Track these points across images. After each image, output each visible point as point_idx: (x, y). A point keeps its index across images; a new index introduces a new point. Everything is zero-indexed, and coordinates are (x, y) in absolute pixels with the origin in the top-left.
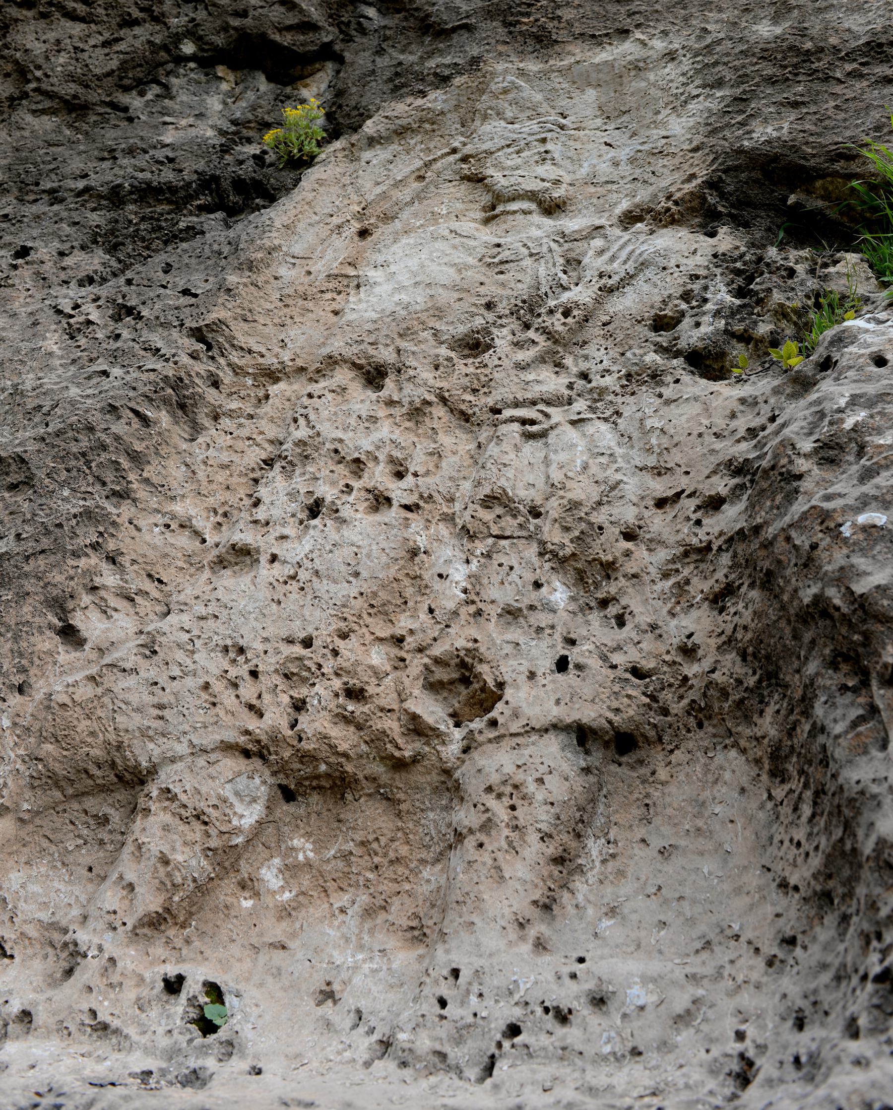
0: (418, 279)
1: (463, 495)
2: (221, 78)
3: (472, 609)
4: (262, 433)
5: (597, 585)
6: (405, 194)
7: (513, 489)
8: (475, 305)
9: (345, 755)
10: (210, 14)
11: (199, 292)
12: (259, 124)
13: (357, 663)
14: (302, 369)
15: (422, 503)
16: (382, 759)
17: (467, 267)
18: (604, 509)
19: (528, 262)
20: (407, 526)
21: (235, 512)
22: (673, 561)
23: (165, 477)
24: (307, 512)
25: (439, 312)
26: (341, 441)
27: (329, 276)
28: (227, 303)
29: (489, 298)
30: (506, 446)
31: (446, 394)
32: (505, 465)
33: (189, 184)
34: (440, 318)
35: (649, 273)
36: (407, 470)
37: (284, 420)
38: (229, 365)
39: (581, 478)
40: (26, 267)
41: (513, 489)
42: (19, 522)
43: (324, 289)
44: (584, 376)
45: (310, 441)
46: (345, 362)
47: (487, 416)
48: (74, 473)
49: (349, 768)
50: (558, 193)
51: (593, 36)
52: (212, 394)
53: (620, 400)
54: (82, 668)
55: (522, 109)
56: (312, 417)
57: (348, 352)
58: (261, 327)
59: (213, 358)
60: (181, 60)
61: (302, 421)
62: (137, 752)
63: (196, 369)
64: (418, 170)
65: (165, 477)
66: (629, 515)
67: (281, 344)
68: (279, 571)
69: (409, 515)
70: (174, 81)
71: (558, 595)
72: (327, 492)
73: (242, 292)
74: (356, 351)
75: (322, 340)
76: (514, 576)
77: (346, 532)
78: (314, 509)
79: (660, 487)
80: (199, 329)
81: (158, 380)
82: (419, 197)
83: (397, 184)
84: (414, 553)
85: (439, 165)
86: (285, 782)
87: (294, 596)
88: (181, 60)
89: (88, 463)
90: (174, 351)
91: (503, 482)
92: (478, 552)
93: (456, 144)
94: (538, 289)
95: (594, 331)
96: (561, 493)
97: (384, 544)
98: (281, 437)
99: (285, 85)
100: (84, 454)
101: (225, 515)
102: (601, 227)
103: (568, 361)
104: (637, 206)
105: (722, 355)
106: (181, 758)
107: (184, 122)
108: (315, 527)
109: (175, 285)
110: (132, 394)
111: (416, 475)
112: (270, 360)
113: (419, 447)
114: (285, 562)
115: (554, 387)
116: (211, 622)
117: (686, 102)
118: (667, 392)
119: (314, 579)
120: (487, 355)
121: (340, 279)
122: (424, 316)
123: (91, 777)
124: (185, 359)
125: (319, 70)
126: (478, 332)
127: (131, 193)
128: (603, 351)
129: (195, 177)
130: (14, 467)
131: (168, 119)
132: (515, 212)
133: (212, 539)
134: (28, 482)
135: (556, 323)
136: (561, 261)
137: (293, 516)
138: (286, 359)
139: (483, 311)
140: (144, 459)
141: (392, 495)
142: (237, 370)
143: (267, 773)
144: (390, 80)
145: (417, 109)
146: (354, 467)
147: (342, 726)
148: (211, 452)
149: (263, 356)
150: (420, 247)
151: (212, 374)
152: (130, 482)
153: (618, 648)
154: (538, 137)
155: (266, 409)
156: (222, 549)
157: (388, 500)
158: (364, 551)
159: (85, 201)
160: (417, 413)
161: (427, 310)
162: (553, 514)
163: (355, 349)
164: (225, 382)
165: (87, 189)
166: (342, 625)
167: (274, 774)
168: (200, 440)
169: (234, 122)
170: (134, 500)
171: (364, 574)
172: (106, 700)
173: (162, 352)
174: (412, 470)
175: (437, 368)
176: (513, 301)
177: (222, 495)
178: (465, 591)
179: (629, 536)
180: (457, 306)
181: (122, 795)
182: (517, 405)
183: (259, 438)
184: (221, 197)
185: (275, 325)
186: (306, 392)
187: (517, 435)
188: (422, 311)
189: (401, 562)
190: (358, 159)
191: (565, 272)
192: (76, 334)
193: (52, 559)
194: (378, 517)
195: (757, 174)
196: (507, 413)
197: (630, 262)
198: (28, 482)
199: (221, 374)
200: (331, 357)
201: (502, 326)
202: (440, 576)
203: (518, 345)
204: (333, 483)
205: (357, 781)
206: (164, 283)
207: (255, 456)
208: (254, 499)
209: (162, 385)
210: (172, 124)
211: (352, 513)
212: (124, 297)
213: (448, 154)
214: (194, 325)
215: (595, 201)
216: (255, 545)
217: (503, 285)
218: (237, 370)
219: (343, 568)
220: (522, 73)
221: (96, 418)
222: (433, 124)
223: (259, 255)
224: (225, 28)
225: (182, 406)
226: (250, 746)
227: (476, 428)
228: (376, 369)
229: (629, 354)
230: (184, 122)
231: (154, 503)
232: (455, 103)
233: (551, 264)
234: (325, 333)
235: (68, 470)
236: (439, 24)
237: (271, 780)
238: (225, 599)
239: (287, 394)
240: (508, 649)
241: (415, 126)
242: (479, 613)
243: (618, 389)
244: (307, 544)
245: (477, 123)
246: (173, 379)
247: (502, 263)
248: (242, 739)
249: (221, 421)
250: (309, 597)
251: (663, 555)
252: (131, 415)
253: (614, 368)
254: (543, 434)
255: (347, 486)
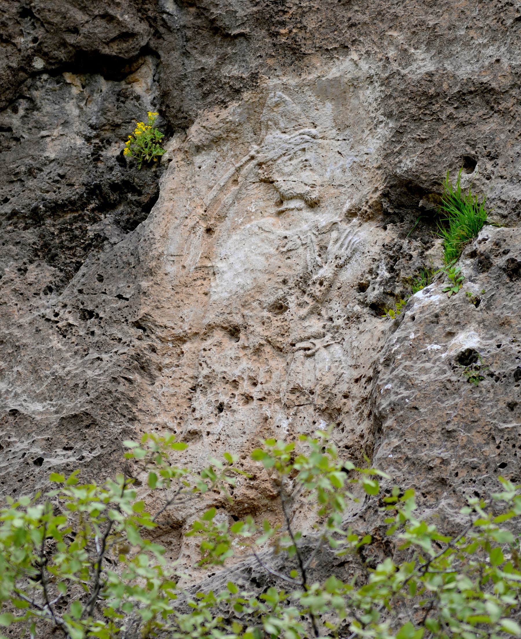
0: (246, 267)
1: (283, 389)
2: (70, 84)
3: (291, 437)
4: (186, 374)
5: (336, 418)
6: (227, 198)
7: (302, 384)
8: (277, 282)
9: (253, 499)
10: (47, 31)
11: (128, 296)
12: (112, 126)
13: (251, 467)
14: (196, 334)
15: (266, 397)
16: (267, 497)
17: (271, 256)
18: (337, 387)
19: (301, 250)
20: (262, 408)
21: (185, 416)
22: (359, 404)
23: (148, 406)
24: (218, 410)
25: (259, 289)
26: (225, 372)
27: (196, 268)
28: (146, 302)
29: (283, 277)
30: (298, 363)
31: (270, 339)
32: (298, 373)
33: (82, 196)
34: (261, 293)
35: (357, 256)
36: (258, 382)
37: (195, 365)
38: (157, 338)
39: (328, 374)
40: (4, 286)
41: (302, 384)
42: (99, 441)
43: (195, 278)
44: (331, 319)
45: (210, 375)
46: (218, 326)
47: (289, 348)
48: (112, 415)
49: (256, 503)
50: (314, 195)
51: (327, 50)
52: (153, 357)
53: (344, 332)
54: (144, 492)
55: (290, 120)
56: (209, 362)
57: (219, 320)
58: (168, 310)
59: (148, 336)
60: (36, 74)
61: (204, 365)
62: (176, 516)
63: (143, 346)
64: (233, 175)
65: (148, 406)
66: (344, 387)
67: (181, 319)
68: (212, 438)
69: (262, 403)
70: (36, 94)
71: (322, 425)
72: (224, 399)
73: (152, 292)
74: (222, 320)
75: (202, 314)
76: (306, 421)
77: (236, 416)
78: (220, 408)
79: (356, 374)
80: (137, 322)
81: (129, 358)
82: (237, 198)
83: (223, 189)
84: (266, 419)
85: (244, 171)
86: (233, 514)
87: (221, 447)
88: (36, 74)
89: (115, 408)
90: (129, 339)
91: (298, 381)
92: (291, 414)
93: (252, 153)
94: (307, 268)
95: (334, 293)
96: (321, 382)
97: (253, 418)
98: (196, 374)
99: (119, 80)
100: (112, 405)
101: (181, 418)
102: (336, 223)
103: (323, 312)
104: (353, 206)
105: (383, 305)
106: (194, 514)
107: (56, 133)
108: (223, 416)
109: (111, 293)
110: (120, 369)
111: (262, 383)
112: (178, 331)
113: (261, 369)
114: (213, 434)
115: (316, 329)
116: (190, 464)
117: (376, 125)
118: (361, 327)
119: (228, 438)
120: (286, 313)
121: (203, 269)
122: (252, 292)
123: (161, 529)
124: (137, 343)
125: (142, 64)
126: (281, 300)
127: (46, 212)
128: (338, 305)
129: (84, 188)
130: (84, 418)
131: (44, 133)
132: (293, 209)
133: (178, 431)
134: (94, 423)
135: (317, 291)
136: (317, 248)
137: (212, 413)
138: (186, 329)
139: (282, 286)
140: (136, 400)
141: (253, 395)
142: (162, 340)
143: (226, 512)
144: (200, 86)
145: (223, 121)
146: (233, 384)
147: (250, 490)
148: (164, 389)
149: (173, 329)
150: (244, 242)
151: (150, 346)
152: (134, 413)
153: (341, 440)
154: (301, 147)
155: (183, 360)
156: (184, 434)
157: (252, 397)
158: (246, 423)
159: (16, 223)
160: (258, 351)
161: (253, 288)
162: (318, 392)
163: (221, 318)
164: (159, 348)
165: (14, 213)
166: (243, 454)
167: (229, 512)
168: (157, 383)
169: (92, 127)
170: (139, 420)
171: (247, 432)
172: (158, 501)
173: (124, 340)
174: (260, 382)
175: (263, 324)
176: (295, 278)
177: (176, 410)
178: (288, 431)
179: (346, 397)
180: (268, 284)
181: (174, 533)
182: (302, 340)
183: (185, 377)
184: (104, 198)
185: (174, 307)
186: (202, 348)
187: (302, 357)
188: (252, 289)
189: (262, 424)
190: (191, 163)
191: (320, 255)
192: (65, 334)
193: (119, 453)
194: (248, 406)
195: (404, 189)
196: (298, 345)
197: (349, 249)
198: (94, 423)
199: (155, 344)
200: (210, 325)
201: (292, 294)
202: (278, 426)
203: (300, 305)
204: (226, 394)
205: (259, 507)
206: (103, 291)
207: (186, 386)
208: (192, 409)
209: (131, 360)
210: (48, 136)
211: (237, 407)
212: (83, 304)
213: (249, 160)
214: (134, 320)
215: (333, 200)
216: (199, 429)
217: (290, 267)
218: (162, 340)
219: (238, 431)
220: (286, 88)
221: (110, 386)
222: (236, 133)
223: (154, 264)
224: (64, 44)
225: (143, 368)
226: (218, 504)
227: (285, 355)
228: (234, 328)
229: (348, 306)
230: (56, 133)
231: (147, 419)
232: (247, 115)
233: (312, 251)
234: (203, 309)
235: (109, 414)
236: (224, 29)
237: (228, 514)
238: (193, 454)
239: (193, 349)
240: (305, 449)
241: (224, 136)
242: (294, 438)
243: (344, 326)
244: (221, 425)
245: (263, 132)
246: (135, 355)
247: (289, 251)
248: (214, 503)
249: (163, 371)
250: (227, 446)
251: (356, 402)
252: (124, 380)
253: (342, 315)
254: (313, 355)
255: (233, 394)
